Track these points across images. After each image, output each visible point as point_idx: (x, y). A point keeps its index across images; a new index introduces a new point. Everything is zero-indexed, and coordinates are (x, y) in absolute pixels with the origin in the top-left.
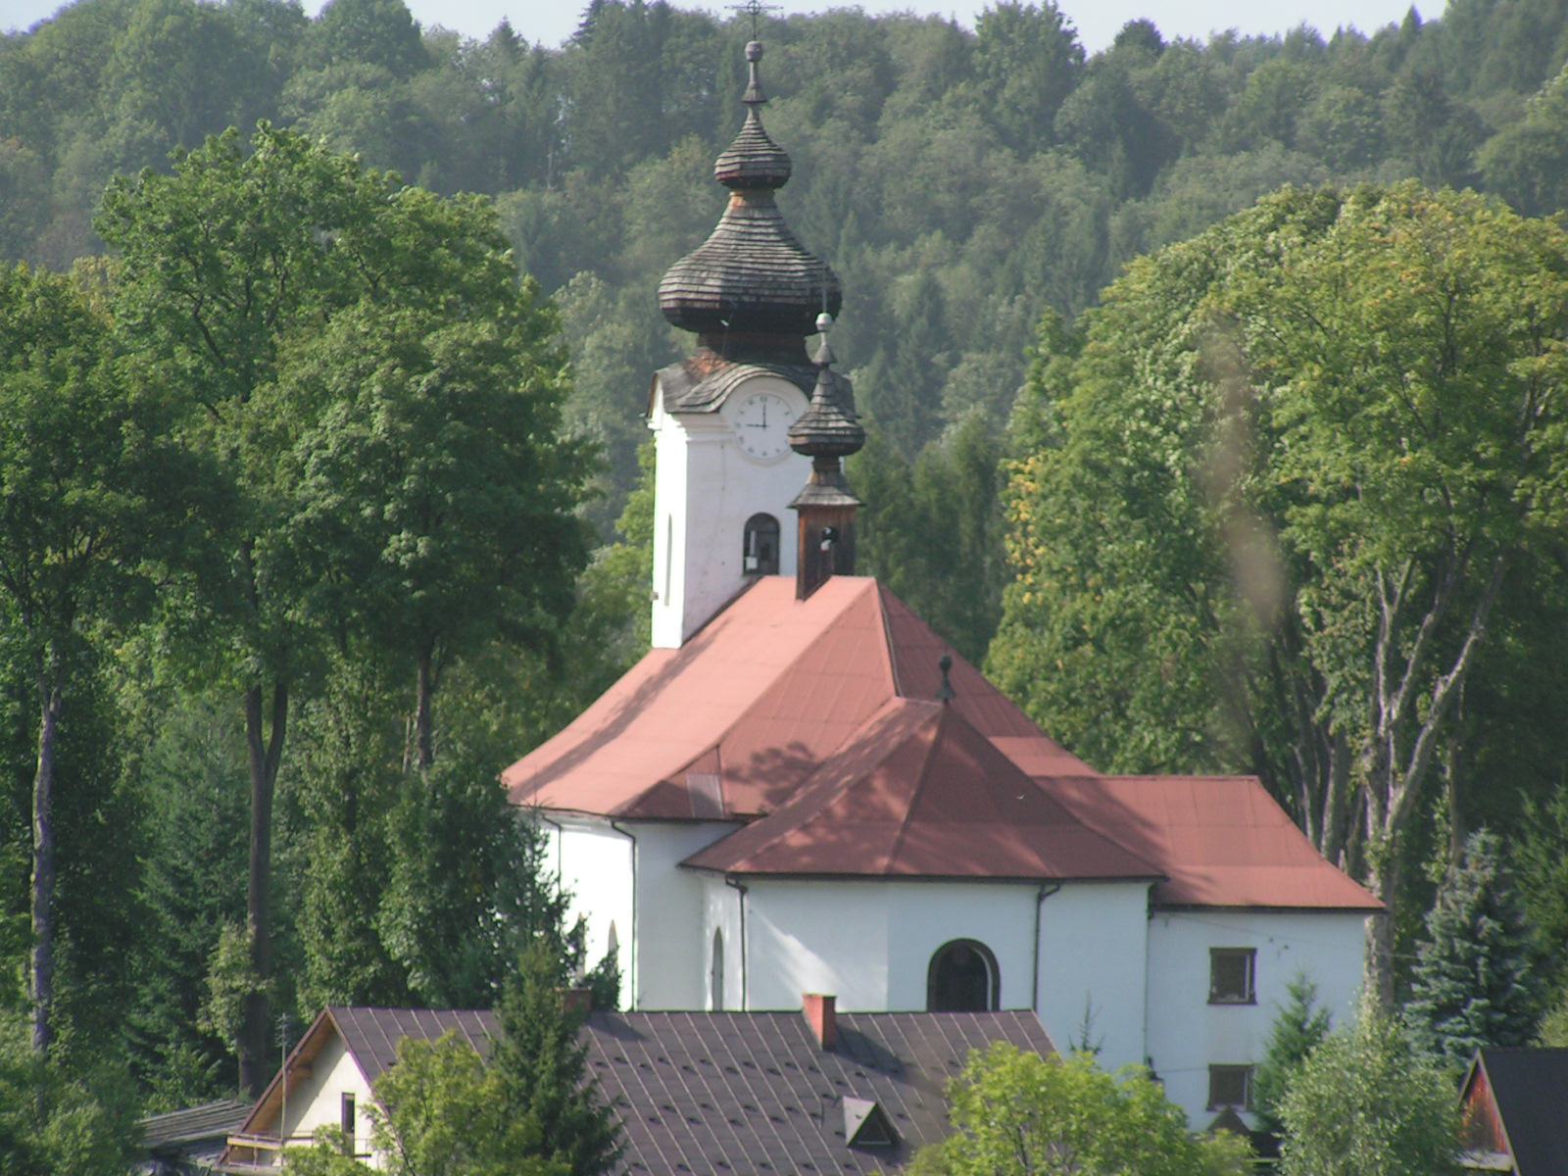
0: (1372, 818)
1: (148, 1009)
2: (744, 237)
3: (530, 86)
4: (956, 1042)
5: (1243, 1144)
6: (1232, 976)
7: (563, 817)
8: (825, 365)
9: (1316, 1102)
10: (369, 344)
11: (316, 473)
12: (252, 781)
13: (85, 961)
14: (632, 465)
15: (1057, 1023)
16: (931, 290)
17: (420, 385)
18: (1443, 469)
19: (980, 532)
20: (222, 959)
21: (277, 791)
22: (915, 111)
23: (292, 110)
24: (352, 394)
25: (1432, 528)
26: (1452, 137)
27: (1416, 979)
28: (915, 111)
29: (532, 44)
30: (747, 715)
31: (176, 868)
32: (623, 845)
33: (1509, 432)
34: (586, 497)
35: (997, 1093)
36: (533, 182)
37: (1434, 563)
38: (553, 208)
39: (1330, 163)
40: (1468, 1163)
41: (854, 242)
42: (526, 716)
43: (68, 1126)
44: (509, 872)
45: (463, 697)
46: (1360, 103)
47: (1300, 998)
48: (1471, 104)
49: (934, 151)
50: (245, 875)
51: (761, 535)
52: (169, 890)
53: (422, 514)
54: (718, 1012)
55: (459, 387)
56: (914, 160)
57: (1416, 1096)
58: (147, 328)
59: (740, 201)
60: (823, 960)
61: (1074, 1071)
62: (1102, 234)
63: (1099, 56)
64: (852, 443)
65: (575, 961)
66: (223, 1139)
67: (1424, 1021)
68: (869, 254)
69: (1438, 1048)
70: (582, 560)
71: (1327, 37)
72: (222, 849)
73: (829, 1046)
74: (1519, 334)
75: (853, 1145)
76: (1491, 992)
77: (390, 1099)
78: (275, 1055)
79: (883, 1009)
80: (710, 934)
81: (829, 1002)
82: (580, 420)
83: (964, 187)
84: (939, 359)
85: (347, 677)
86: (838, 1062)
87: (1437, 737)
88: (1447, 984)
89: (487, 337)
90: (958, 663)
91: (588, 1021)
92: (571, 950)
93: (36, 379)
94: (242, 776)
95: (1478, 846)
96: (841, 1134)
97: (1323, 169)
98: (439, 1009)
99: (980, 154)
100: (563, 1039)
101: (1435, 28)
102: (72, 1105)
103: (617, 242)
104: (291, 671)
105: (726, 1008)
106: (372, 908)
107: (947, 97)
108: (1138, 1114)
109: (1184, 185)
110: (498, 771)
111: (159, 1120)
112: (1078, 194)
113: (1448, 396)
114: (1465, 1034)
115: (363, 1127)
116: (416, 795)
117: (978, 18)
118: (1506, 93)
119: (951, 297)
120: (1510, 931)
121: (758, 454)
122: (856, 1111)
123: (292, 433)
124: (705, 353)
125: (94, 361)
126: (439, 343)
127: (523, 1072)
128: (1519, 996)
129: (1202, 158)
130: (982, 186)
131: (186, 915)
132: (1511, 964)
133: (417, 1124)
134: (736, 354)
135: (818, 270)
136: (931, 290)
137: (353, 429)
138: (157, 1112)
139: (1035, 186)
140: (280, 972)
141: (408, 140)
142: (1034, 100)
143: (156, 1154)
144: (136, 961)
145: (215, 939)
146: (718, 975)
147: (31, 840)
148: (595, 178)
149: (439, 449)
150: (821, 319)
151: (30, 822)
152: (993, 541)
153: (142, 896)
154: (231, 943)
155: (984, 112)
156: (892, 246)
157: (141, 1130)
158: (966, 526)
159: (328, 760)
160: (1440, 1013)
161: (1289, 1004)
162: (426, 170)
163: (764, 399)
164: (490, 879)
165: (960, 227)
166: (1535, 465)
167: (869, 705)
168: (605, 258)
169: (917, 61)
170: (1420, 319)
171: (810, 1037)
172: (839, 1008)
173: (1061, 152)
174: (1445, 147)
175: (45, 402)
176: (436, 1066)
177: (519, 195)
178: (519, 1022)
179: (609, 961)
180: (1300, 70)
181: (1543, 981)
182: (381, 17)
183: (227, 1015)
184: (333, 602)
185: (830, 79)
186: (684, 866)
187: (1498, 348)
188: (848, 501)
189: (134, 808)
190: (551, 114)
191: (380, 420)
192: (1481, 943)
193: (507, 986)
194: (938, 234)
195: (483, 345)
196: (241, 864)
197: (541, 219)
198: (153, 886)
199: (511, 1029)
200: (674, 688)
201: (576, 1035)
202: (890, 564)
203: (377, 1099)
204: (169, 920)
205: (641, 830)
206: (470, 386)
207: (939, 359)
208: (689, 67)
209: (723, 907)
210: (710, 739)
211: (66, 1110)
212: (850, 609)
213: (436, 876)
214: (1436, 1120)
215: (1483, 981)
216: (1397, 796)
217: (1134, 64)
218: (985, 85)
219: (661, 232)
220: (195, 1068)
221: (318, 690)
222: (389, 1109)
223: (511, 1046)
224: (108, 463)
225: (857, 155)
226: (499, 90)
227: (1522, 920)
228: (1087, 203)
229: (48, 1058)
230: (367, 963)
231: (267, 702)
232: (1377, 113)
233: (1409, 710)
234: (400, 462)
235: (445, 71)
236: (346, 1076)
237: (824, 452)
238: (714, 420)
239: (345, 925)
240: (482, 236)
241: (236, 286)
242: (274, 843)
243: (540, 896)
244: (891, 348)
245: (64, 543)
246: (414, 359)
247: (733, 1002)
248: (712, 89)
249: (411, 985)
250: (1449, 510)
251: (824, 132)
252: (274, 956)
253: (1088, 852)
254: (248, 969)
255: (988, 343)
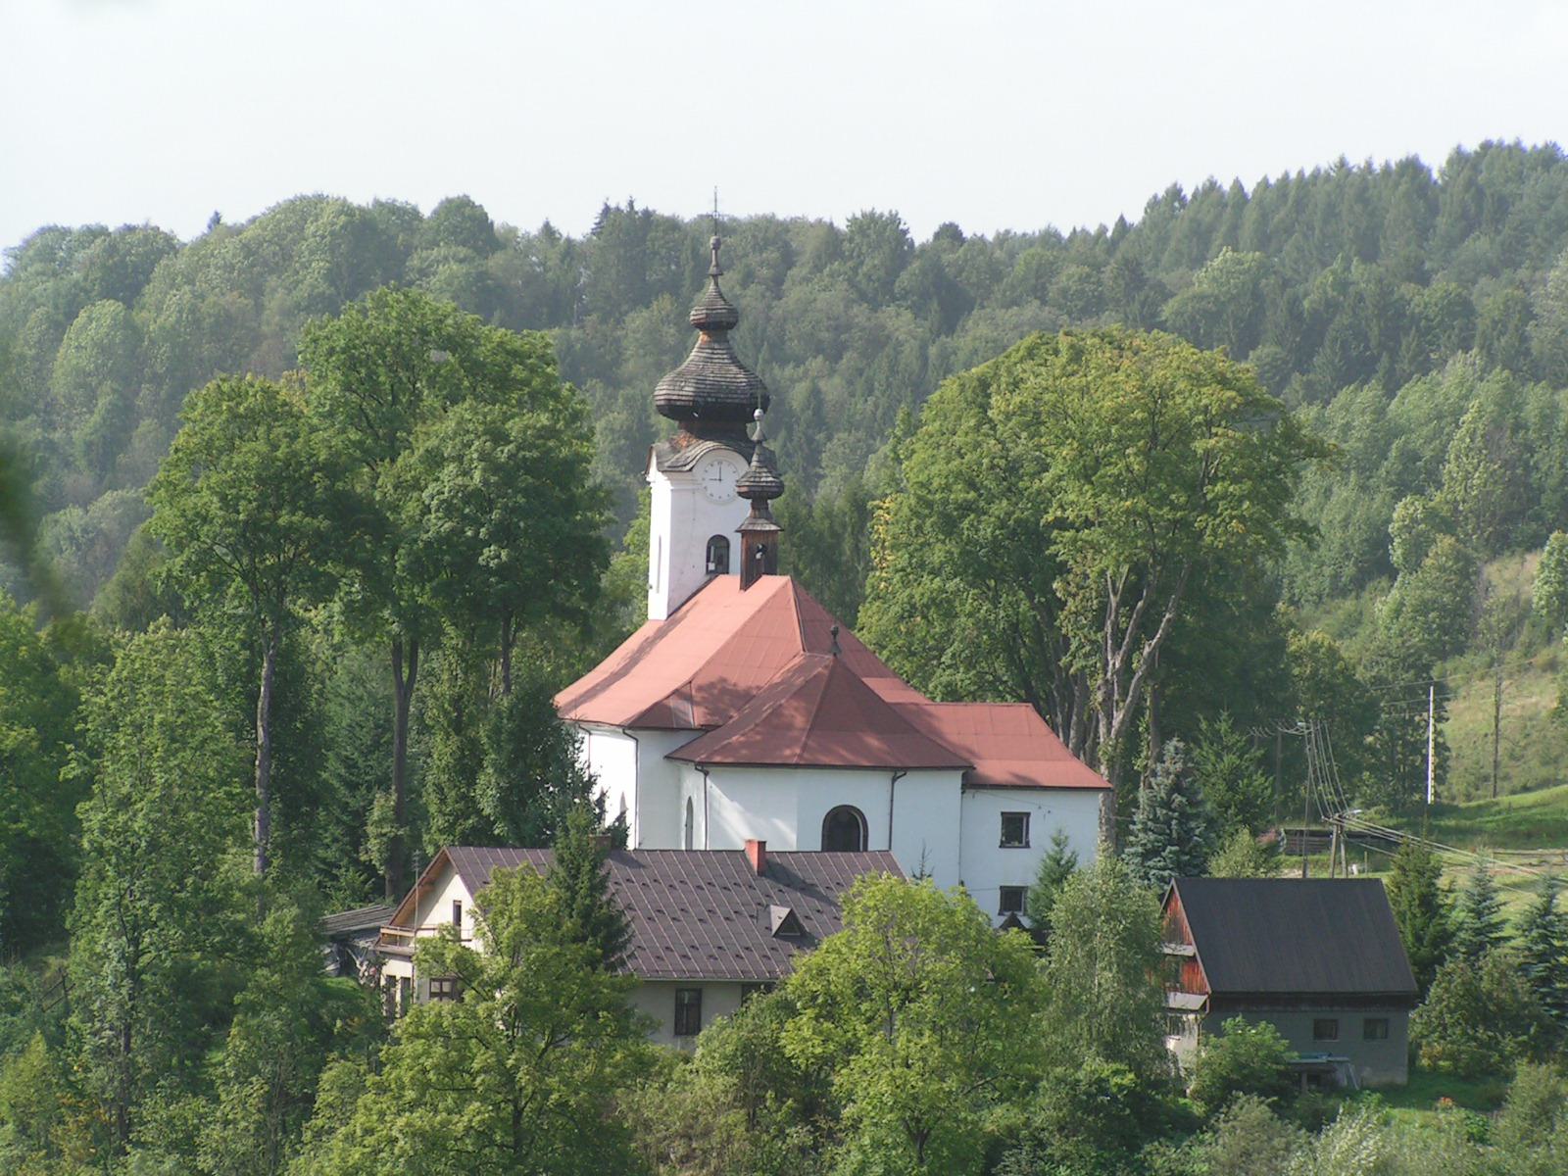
0: (1102, 730)
1: (328, 846)
2: (708, 360)
3: (562, 261)
4: (842, 870)
5: (1026, 937)
6: (1015, 830)
7: (591, 726)
8: (759, 442)
9: (1071, 910)
10: (471, 426)
11: (437, 511)
12: (396, 702)
13: (289, 816)
14: (632, 505)
15: (905, 858)
16: (815, 393)
17: (503, 453)
18: (1152, 510)
19: (856, 549)
20: (376, 814)
21: (412, 709)
22: (807, 280)
23: (412, 276)
24: (460, 459)
25: (1144, 547)
26: (1147, 297)
27: (1131, 833)
28: (807, 280)
29: (565, 235)
30: (708, 663)
31: (347, 757)
32: (629, 745)
33: (1194, 487)
34: (605, 523)
35: (871, 904)
36: (565, 323)
37: (1138, 569)
38: (578, 339)
39: (1069, 314)
40: (1167, 951)
41: (767, 362)
42: (567, 661)
43: (277, 921)
44: (558, 760)
45: (527, 652)
46: (1088, 276)
47: (1058, 845)
48: (1159, 277)
49: (819, 305)
50: (391, 762)
51: (718, 548)
52: (343, 771)
53: (503, 534)
54: (689, 851)
55: (528, 454)
56: (806, 311)
57: (1134, 908)
58: (331, 414)
59: (706, 338)
60: (746, 817)
61: (924, 891)
62: (924, 358)
63: (923, 245)
64: (777, 491)
65: (600, 818)
66: (379, 928)
67: (1138, 860)
68: (777, 371)
69: (1146, 876)
70: (606, 564)
71: (1066, 234)
72: (376, 745)
73: (761, 873)
74: (1198, 425)
75: (776, 935)
76: (1180, 842)
77: (484, 906)
78: (410, 876)
79: (794, 849)
80: (685, 803)
81: (762, 845)
82: (601, 470)
83: (836, 328)
84: (820, 437)
85: (452, 636)
86: (767, 882)
87: (1144, 679)
88: (1152, 837)
89: (546, 423)
90: (842, 630)
91: (609, 856)
92: (597, 811)
93: (262, 447)
94: (388, 698)
95: (1172, 749)
96: (769, 929)
97: (1065, 317)
98: (514, 847)
99: (847, 307)
100: (594, 868)
101: (1139, 230)
102: (281, 908)
103: (618, 361)
104: (419, 633)
105: (695, 847)
106: (471, 783)
107: (827, 271)
108: (960, 917)
109: (976, 328)
110: (552, 697)
111: (335, 917)
112: (910, 333)
113: (1156, 466)
114: (1164, 869)
115: (467, 923)
116: (499, 714)
117: (631, 204)
118: (1182, 270)
119: (829, 397)
120: (1191, 803)
121: (716, 497)
122: (778, 914)
123: (423, 483)
124: (682, 434)
125: (297, 436)
126: (514, 427)
127: (568, 888)
128: (1198, 844)
129: (988, 310)
130: (848, 328)
131: (353, 787)
132: (1193, 824)
133: (503, 922)
134: (703, 435)
135: (755, 383)
136: (815, 393)
137: (460, 480)
138: (333, 912)
139: (883, 327)
140: (412, 823)
141: (485, 295)
142: (882, 273)
143: (333, 939)
144: (322, 814)
145: (371, 802)
146: (690, 826)
147: (256, 739)
148: (604, 321)
149: (516, 493)
150: (757, 413)
151: (255, 728)
152: (864, 553)
153: (325, 775)
154: (382, 805)
155: (850, 281)
156: (791, 365)
157: (325, 923)
158: (847, 546)
159: (443, 689)
160: (1147, 855)
161: (1051, 848)
162: (497, 314)
163: (720, 463)
164: (546, 765)
165: (835, 354)
166: (1209, 508)
167: (783, 655)
168: (610, 375)
169: (808, 248)
170: (1139, 415)
171: (749, 866)
172: (768, 849)
173: (899, 306)
174: (1143, 304)
175: (267, 461)
176: (515, 884)
177: (556, 331)
178: (566, 856)
179: (621, 818)
180: (1049, 255)
181: (1213, 835)
182: (469, 217)
183: (379, 850)
184: (444, 590)
185: (753, 259)
186: (667, 757)
187: (1184, 432)
188: (773, 528)
189: (322, 719)
190: (576, 280)
191: (477, 475)
192: (1174, 811)
193: (558, 832)
194: (820, 358)
195: (544, 427)
196: (389, 754)
197: (570, 347)
198: (332, 771)
199: (561, 861)
200: (661, 645)
201: (602, 865)
202: (801, 566)
203: (479, 906)
204: (343, 790)
205: (640, 734)
206: (536, 454)
207: (820, 437)
208: (663, 252)
209: (693, 783)
210: (686, 678)
211: (277, 910)
212: (774, 596)
213: (512, 764)
214: (1146, 922)
215: (1175, 835)
216: (1118, 716)
217: (945, 250)
218: (850, 264)
219: (645, 355)
220: (357, 884)
221: (438, 645)
222: (485, 912)
223: (562, 872)
224: (306, 499)
225: (770, 307)
226: (542, 264)
227: (1200, 797)
228: (915, 338)
229: (265, 878)
230: (468, 818)
231: (406, 648)
232: (1099, 283)
233: (1127, 662)
234: (491, 502)
235: (511, 252)
236: (456, 889)
237: (758, 497)
238: (688, 476)
239: (453, 793)
240: (542, 357)
241: (383, 388)
242: (409, 742)
243: (578, 776)
244: (790, 430)
245: (277, 549)
246: (499, 437)
247: (700, 843)
248: (677, 264)
249: (496, 832)
250: (1154, 536)
251: (749, 292)
252: (409, 813)
253: (911, 750)
254: (392, 821)
255: (852, 426)
